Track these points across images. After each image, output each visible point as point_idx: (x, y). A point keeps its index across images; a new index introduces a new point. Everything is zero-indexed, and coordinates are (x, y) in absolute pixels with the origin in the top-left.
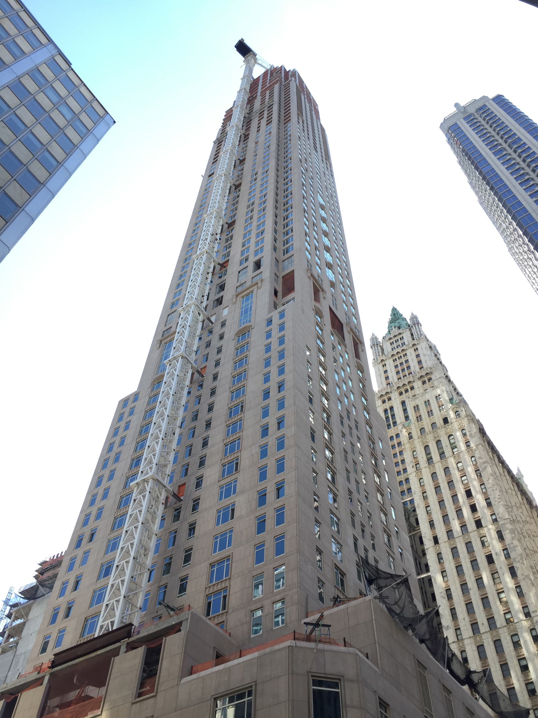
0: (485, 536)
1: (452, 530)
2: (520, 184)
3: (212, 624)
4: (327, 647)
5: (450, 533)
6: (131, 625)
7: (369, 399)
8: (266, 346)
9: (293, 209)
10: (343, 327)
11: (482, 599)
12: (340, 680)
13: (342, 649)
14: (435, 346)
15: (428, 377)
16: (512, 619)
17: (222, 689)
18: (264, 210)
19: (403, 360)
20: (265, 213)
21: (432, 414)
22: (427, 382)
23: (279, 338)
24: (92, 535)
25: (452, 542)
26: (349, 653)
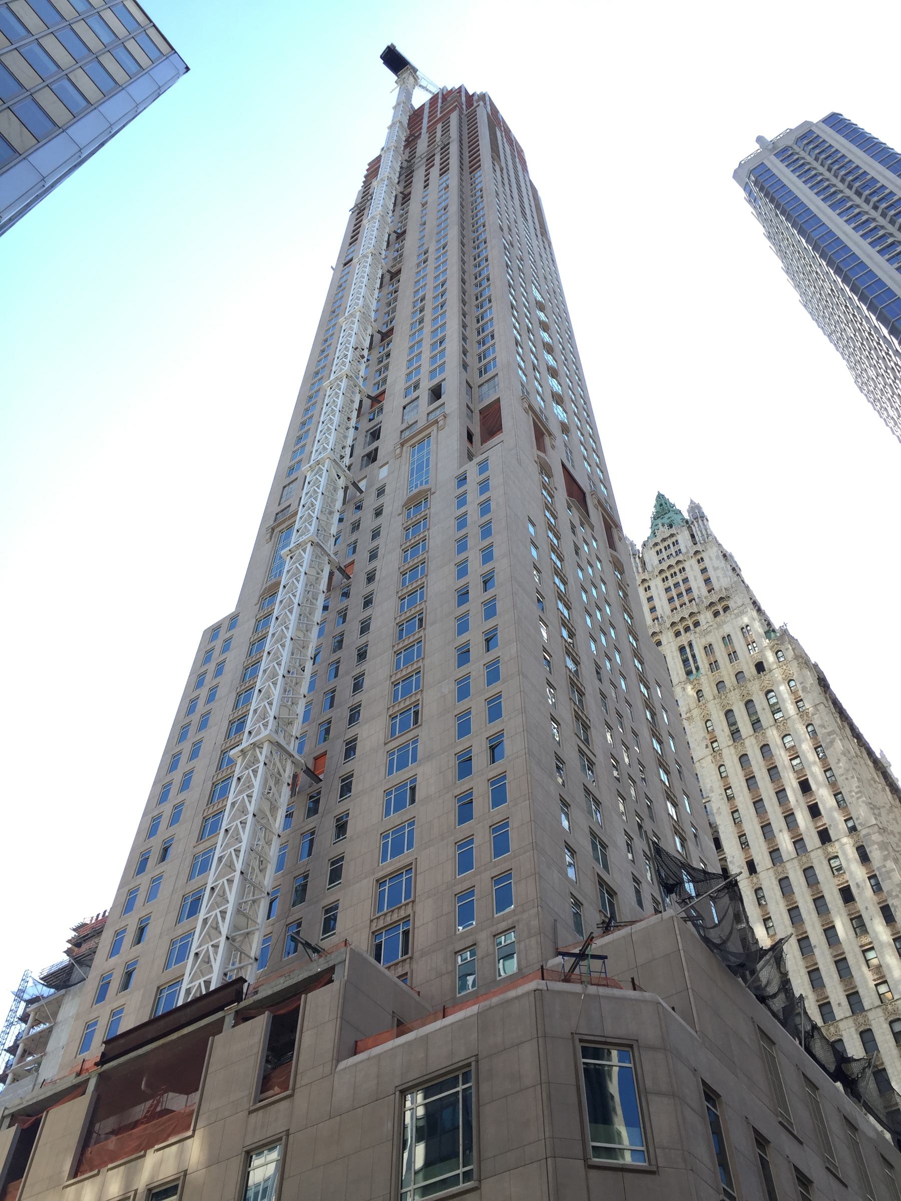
0: (837, 857)
1: (778, 849)
2: (879, 252)
3: (392, 975)
4: (602, 991)
5: (775, 853)
6: (242, 980)
7: (634, 615)
8: (457, 518)
9: (493, 303)
10: (585, 497)
11: (836, 962)
12: (631, 1046)
13: (631, 993)
14: (731, 556)
15: (723, 604)
16: (889, 995)
17: (414, 1075)
18: (442, 307)
19: (679, 578)
20: (445, 311)
21: (737, 658)
22: (722, 612)
23: (481, 504)
24: (166, 850)
25: (780, 869)
26: (645, 1001)
